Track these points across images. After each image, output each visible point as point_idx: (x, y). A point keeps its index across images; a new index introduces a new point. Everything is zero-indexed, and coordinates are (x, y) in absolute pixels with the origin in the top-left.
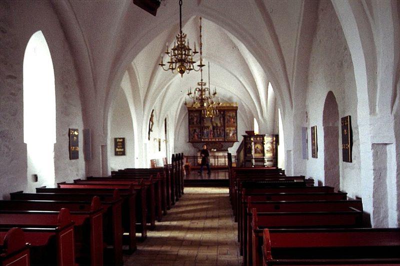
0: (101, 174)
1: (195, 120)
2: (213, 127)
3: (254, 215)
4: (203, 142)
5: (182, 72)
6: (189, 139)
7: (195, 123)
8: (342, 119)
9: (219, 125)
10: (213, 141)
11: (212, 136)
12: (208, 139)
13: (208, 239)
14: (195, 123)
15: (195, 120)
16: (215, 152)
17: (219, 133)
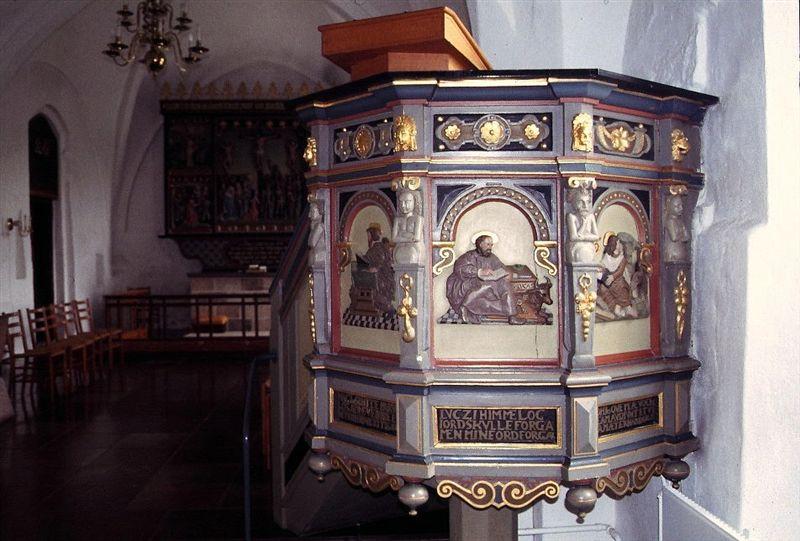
0: (677, 386)
1: (190, 151)
2: (263, 181)
3: (627, 289)
4: (221, 236)
5: (190, 21)
6: (167, 225)
7: (190, 163)
8: (443, 439)
9: (284, 171)
10: (261, 235)
11: (256, 212)
12: (242, 226)
13: (484, 393)
14: (190, 163)
15: (190, 151)
16: (262, 274)
17: (282, 201)
